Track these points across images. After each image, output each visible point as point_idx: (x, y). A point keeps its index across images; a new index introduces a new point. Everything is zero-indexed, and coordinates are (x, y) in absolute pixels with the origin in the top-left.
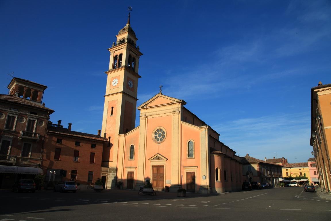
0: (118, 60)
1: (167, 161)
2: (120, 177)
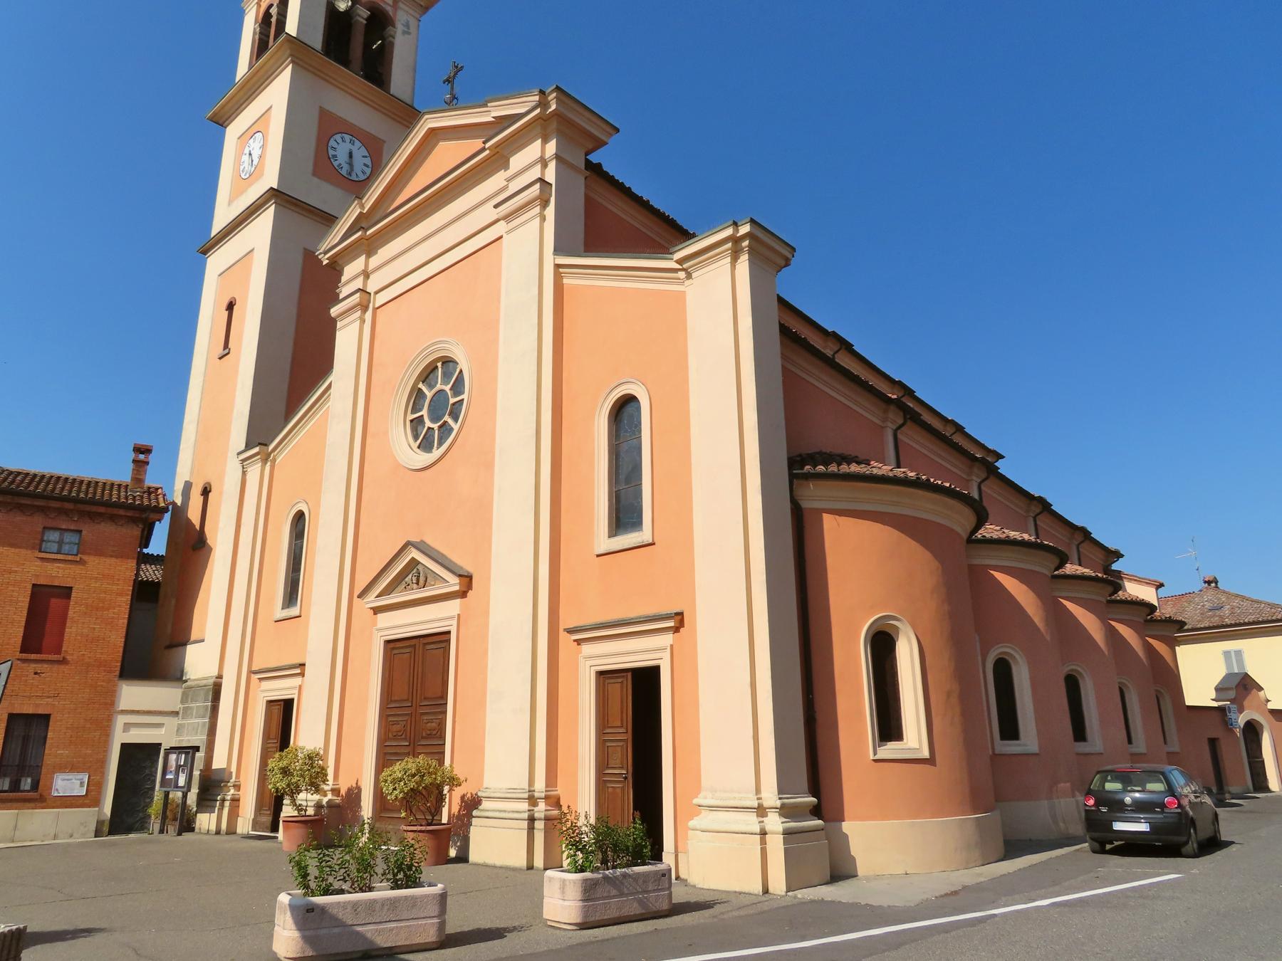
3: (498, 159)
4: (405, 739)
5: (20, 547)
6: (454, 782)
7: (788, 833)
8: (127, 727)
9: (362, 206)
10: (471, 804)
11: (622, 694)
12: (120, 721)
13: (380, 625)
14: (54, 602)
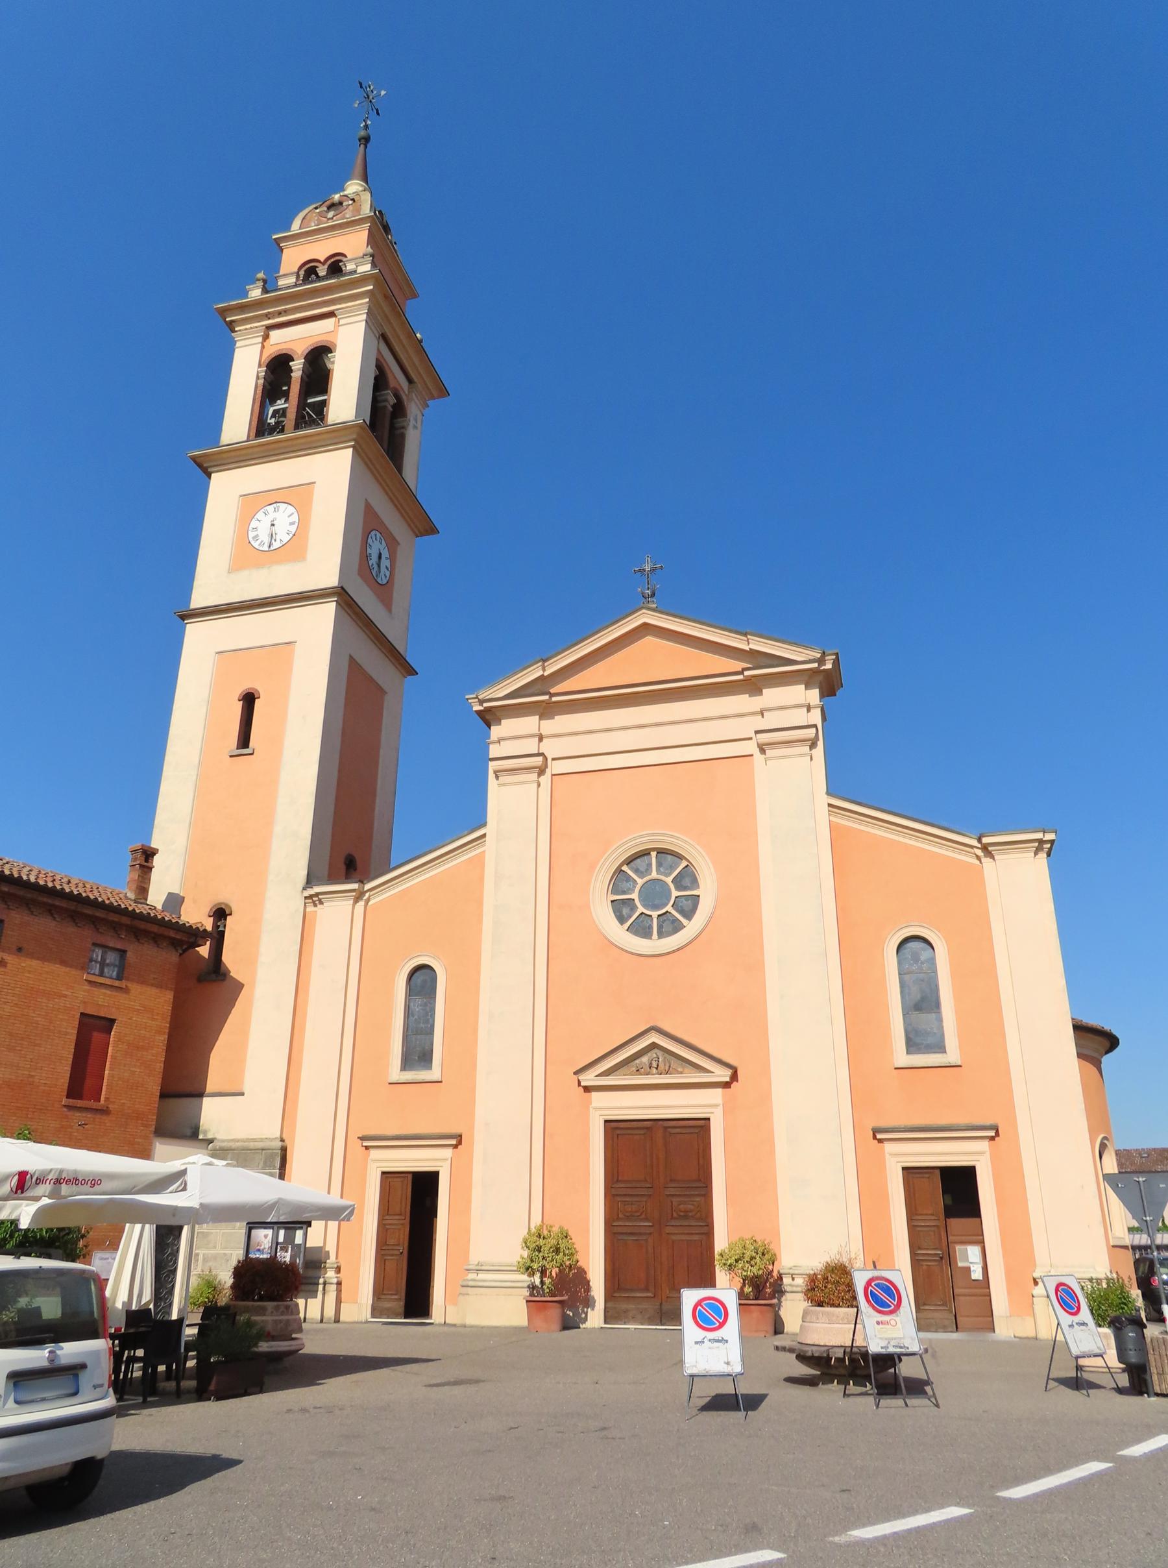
0: (295, 389)
2: (361, 189)
4: (646, 1219)
5: (71, 967)
9: (544, 670)
11: (405, 1192)
13: (594, 1104)
14: (97, 1036)
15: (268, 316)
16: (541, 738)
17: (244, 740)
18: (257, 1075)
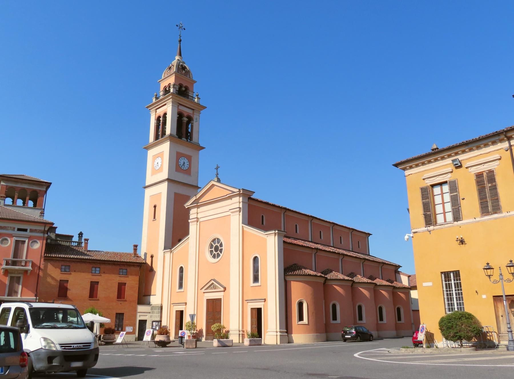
1: (224, 291)
3: (230, 198)
6: (224, 328)
7: (280, 335)
8: (140, 316)
10: (228, 332)
11: (255, 312)
12: (138, 314)
14: (123, 287)
15: (155, 107)
16: (197, 213)
17: (154, 218)
18: (161, 291)
